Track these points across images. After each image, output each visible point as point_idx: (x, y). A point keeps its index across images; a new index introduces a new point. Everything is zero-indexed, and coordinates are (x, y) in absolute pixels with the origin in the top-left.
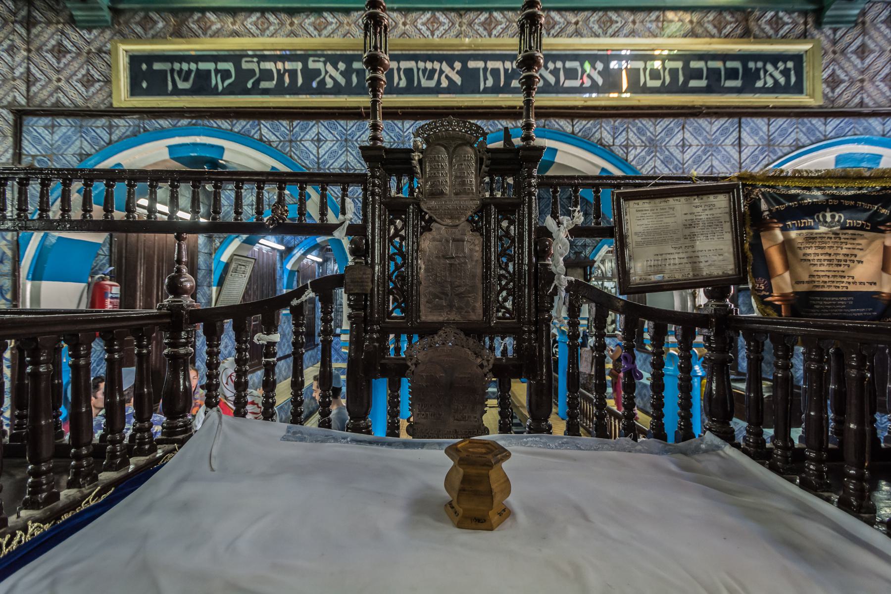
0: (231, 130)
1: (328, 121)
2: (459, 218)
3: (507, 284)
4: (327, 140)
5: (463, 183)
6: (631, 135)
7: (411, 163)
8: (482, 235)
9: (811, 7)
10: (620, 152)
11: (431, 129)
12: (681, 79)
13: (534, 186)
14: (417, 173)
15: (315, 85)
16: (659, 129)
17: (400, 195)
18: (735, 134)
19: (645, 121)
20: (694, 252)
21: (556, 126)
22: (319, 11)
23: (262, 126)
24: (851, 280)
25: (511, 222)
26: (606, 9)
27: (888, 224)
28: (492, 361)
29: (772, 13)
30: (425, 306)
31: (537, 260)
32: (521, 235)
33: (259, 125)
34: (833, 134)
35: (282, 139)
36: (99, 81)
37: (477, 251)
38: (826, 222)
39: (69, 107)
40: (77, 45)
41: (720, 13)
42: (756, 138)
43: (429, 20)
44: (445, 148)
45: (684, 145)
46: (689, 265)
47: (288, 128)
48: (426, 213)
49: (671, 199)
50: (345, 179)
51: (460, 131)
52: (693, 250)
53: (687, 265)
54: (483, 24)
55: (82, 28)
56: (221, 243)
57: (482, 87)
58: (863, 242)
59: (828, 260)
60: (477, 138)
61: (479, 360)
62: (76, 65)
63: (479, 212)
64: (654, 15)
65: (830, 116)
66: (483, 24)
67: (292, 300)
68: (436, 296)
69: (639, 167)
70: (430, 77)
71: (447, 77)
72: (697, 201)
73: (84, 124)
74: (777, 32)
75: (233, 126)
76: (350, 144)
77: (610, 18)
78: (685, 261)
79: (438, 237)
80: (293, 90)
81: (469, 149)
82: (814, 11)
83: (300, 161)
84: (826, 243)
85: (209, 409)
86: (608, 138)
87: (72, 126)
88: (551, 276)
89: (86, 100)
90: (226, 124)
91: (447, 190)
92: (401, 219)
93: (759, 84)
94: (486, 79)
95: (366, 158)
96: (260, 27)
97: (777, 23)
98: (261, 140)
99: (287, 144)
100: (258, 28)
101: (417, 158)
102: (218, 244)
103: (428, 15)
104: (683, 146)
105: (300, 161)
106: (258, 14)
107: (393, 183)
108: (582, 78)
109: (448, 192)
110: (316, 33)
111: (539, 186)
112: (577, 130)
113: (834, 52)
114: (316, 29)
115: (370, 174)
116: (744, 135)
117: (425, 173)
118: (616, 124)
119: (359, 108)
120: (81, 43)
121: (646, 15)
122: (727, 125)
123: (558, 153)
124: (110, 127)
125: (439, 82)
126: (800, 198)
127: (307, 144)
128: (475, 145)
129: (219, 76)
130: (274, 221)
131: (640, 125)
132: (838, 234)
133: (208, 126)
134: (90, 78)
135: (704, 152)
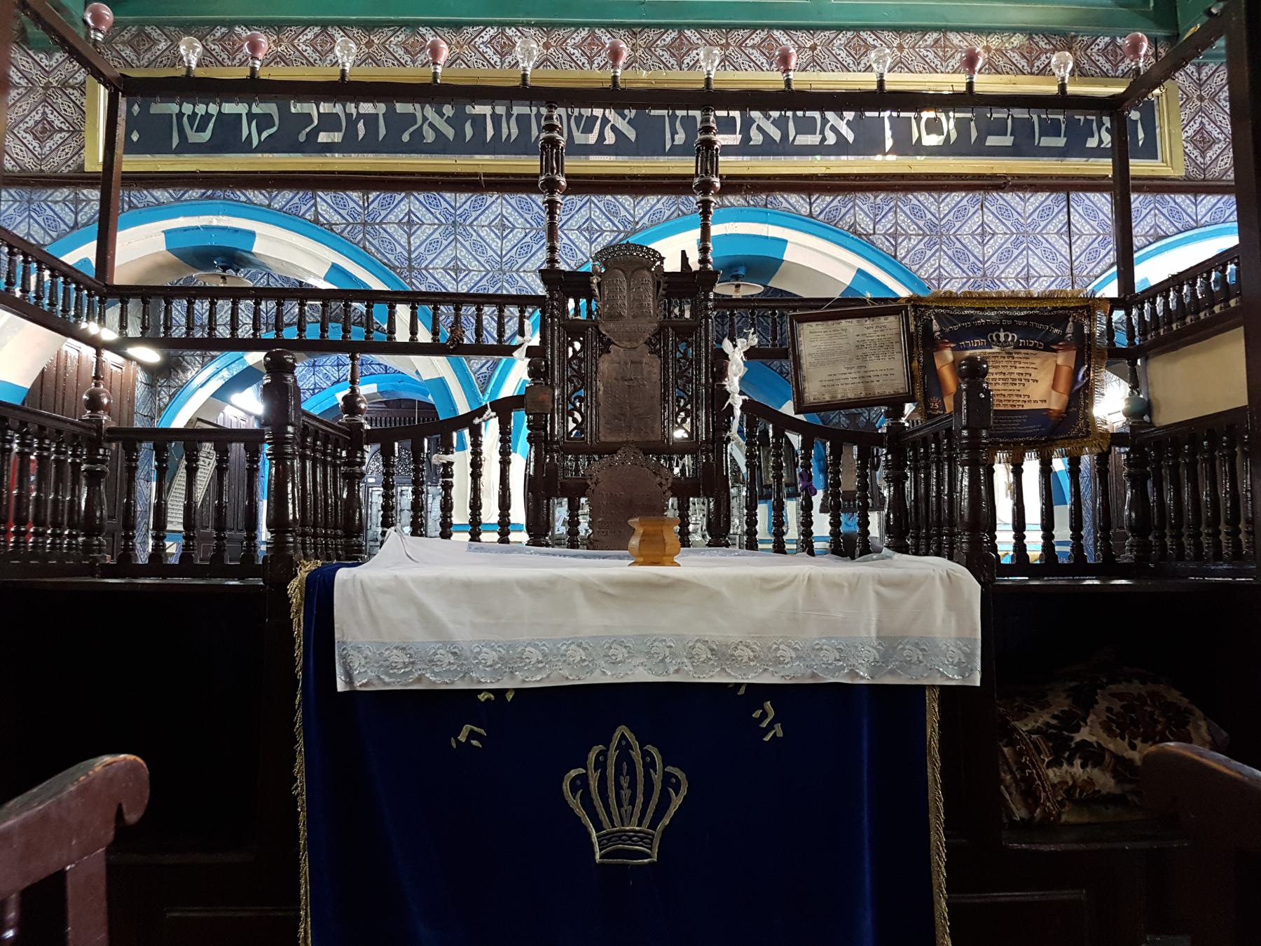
0: (269, 206)
1: (426, 194)
2: (637, 341)
3: (686, 405)
4: (423, 223)
5: (641, 306)
6: (901, 217)
7: (590, 287)
8: (660, 357)
9: (1161, 33)
10: (885, 245)
11: (610, 253)
12: (974, 134)
13: (711, 309)
14: (596, 296)
15: (406, 137)
16: (944, 208)
17: (578, 317)
18: (1063, 217)
19: (923, 196)
20: (866, 372)
21: (785, 204)
22: (413, 26)
23: (318, 199)
24: (1026, 399)
25: (690, 344)
26: (857, 29)
27: (1061, 343)
28: (670, 480)
29: (1107, 39)
30: (604, 427)
31: (714, 381)
32: (698, 355)
33: (314, 198)
34: (1207, 218)
35: (351, 221)
36: (61, 130)
37: (655, 373)
38: (1000, 342)
39: (13, 172)
40: (29, 76)
41: (1031, 38)
42: (1094, 224)
43: (584, 40)
44: (623, 271)
45: (984, 233)
46: (861, 385)
47: (361, 203)
48: (604, 335)
49: (843, 321)
50: (523, 301)
51: (638, 255)
52: (865, 370)
53: (859, 385)
54: (668, 48)
55: (39, 50)
56: (171, 397)
57: (668, 147)
58: (1038, 361)
59: (1003, 379)
60: (655, 262)
61: (658, 479)
62: (25, 106)
63: (657, 334)
64: (930, 38)
65: (1202, 192)
66: (668, 48)
67: (474, 418)
68: (615, 417)
69: (914, 268)
70: (588, 129)
71: (614, 128)
72: (868, 322)
73: (35, 197)
74: (1116, 66)
75: (271, 199)
76: (460, 229)
77: (865, 41)
78: (857, 380)
79: (616, 359)
80: (371, 145)
81: (646, 272)
82: (1167, 38)
83: (379, 256)
84: (999, 362)
85: (385, 529)
86: (865, 224)
87: (15, 201)
88: (727, 395)
89: (41, 159)
90: (261, 197)
91: (625, 313)
92: (580, 341)
93: (1092, 143)
94: (674, 132)
95: (544, 280)
96: (319, 48)
97: (1115, 54)
98: (316, 221)
99: (360, 228)
100: (315, 50)
101: (595, 281)
102: (166, 400)
103: (584, 33)
104: (983, 234)
105: (379, 256)
106: (317, 30)
107: (571, 304)
108: (822, 132)
109: (626, 315)
110: (407, 58)
111: (715, 308)
112: (816, 210)
113: (1201, 98)
114: (407, 51)
115: (548, 296)
116: (1075, 218)
117: (604, 295)
118: (878, 199)
119: (476, 175)
120: (35, 72)
121: (918, 37)
122: (1049, 202)
123: (788, 244)
124: (77, 201)
125: (601, 136)
126: (973, 318)
127: (390, 229)
128: (653, 269)
129: (254, 123)
130: (454, 341)
131: (915, 201)
132: (1011, 353)
133: (232, 200)
134: (47, 126)
135: (1016, 244)
